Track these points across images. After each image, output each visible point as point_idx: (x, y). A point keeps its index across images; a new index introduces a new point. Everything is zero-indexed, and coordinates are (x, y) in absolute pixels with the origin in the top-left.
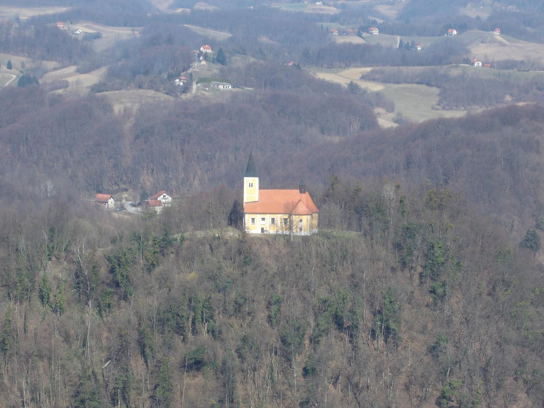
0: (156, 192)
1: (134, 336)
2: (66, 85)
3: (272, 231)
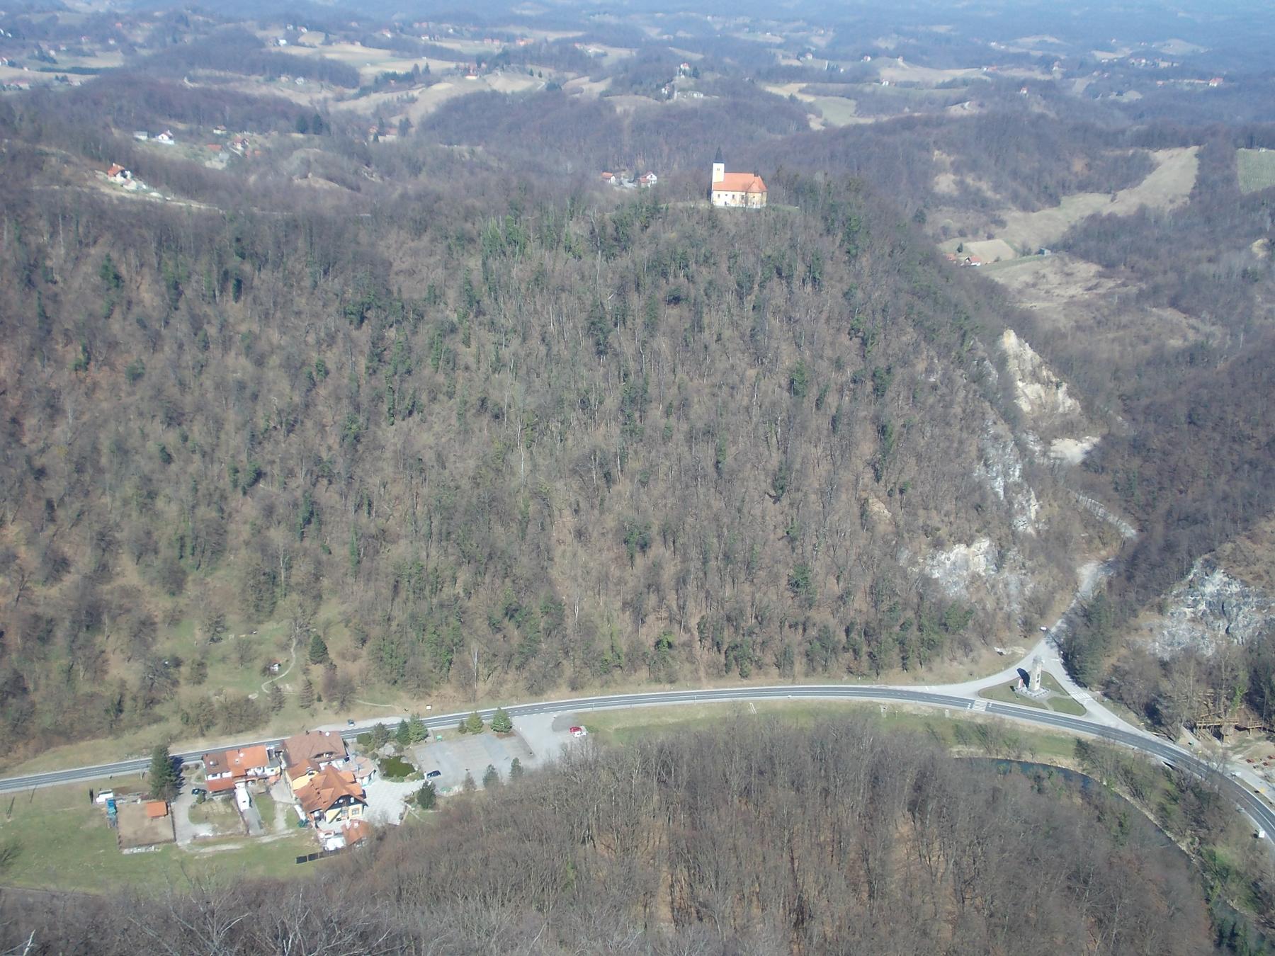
0: (646, 172)
1: (632, 277)
2: (581, 91)
3: (733, 205)
